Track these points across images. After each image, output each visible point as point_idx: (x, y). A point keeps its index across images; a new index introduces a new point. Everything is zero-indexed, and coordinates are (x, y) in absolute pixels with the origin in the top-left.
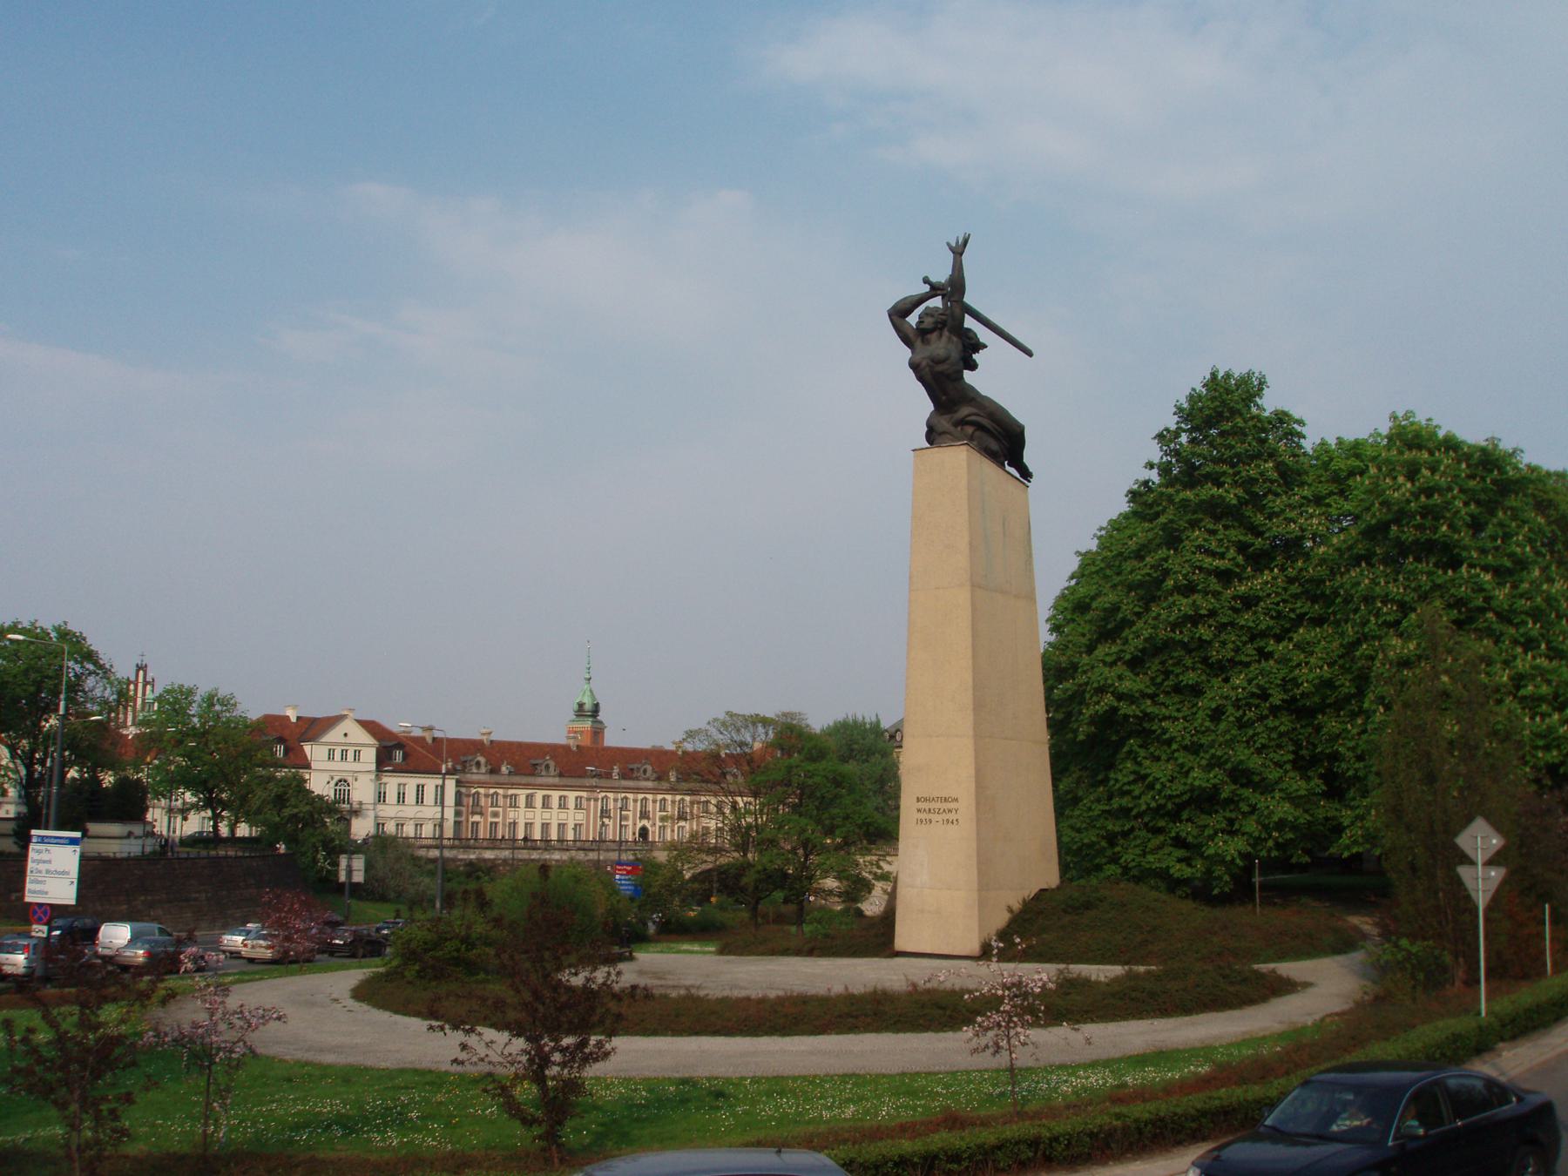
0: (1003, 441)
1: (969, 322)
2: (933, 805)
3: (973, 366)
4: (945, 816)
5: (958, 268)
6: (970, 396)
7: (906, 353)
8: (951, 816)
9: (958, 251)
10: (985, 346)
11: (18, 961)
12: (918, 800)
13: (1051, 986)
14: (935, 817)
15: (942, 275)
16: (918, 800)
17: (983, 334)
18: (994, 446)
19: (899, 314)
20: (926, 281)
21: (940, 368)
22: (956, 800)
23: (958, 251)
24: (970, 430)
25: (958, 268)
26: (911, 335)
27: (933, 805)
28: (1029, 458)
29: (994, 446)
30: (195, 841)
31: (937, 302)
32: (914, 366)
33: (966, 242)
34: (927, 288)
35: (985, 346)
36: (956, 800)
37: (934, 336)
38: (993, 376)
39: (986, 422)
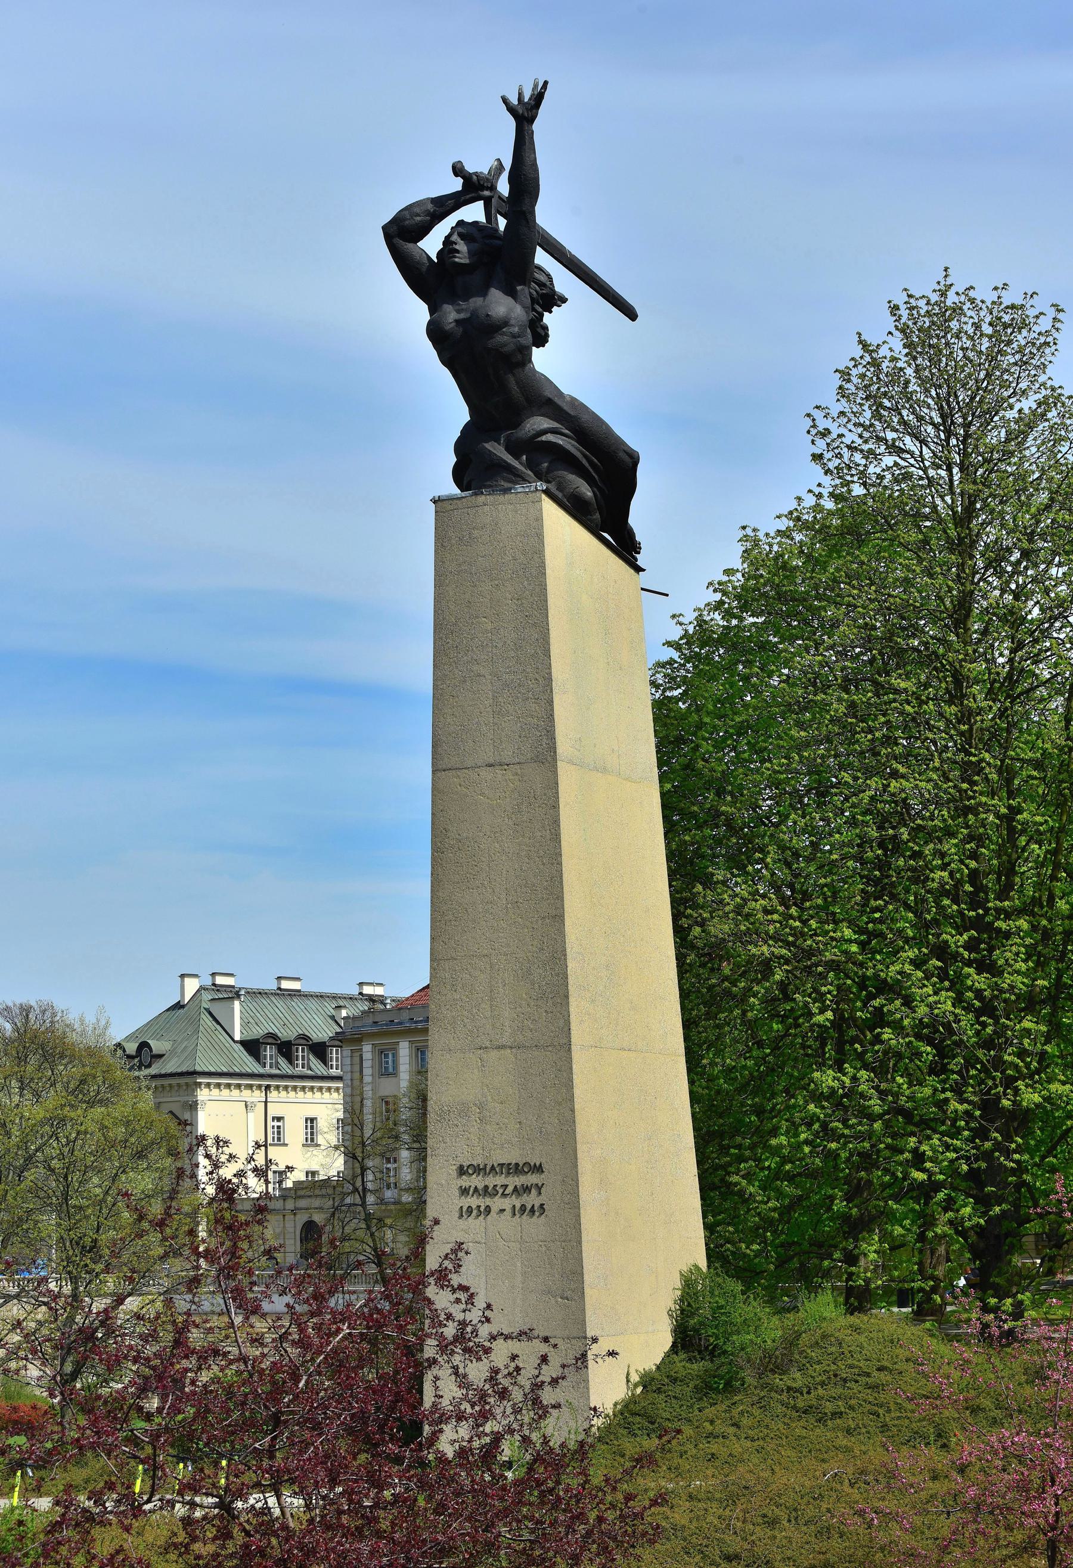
1: (542, 258)
2: (491, 1181)
6: (545, 400)
7: (419, 312)
8: (532, 1199)
9: (525, 113)
10: (564, 300)
11: (1069, 1123)
12: (462, 1171)
13: (1025, 1104)
14: (497, 1203)
15: (490, 149)
16: (462, 1171)
17: (563, 280)
18: (587, 492)
19: (402, 233)
20: (458, 170)
22: (538, 1169)
23: (525, 113)
27: (491, 1181)
28: (640, 516)
29: (587, 492)
31: (474, 212)
32: (435, 332)
33: (538, 98)
34: (456, 185)
35: (564, 300)
36: (538, 1169)
38: (574, 356)
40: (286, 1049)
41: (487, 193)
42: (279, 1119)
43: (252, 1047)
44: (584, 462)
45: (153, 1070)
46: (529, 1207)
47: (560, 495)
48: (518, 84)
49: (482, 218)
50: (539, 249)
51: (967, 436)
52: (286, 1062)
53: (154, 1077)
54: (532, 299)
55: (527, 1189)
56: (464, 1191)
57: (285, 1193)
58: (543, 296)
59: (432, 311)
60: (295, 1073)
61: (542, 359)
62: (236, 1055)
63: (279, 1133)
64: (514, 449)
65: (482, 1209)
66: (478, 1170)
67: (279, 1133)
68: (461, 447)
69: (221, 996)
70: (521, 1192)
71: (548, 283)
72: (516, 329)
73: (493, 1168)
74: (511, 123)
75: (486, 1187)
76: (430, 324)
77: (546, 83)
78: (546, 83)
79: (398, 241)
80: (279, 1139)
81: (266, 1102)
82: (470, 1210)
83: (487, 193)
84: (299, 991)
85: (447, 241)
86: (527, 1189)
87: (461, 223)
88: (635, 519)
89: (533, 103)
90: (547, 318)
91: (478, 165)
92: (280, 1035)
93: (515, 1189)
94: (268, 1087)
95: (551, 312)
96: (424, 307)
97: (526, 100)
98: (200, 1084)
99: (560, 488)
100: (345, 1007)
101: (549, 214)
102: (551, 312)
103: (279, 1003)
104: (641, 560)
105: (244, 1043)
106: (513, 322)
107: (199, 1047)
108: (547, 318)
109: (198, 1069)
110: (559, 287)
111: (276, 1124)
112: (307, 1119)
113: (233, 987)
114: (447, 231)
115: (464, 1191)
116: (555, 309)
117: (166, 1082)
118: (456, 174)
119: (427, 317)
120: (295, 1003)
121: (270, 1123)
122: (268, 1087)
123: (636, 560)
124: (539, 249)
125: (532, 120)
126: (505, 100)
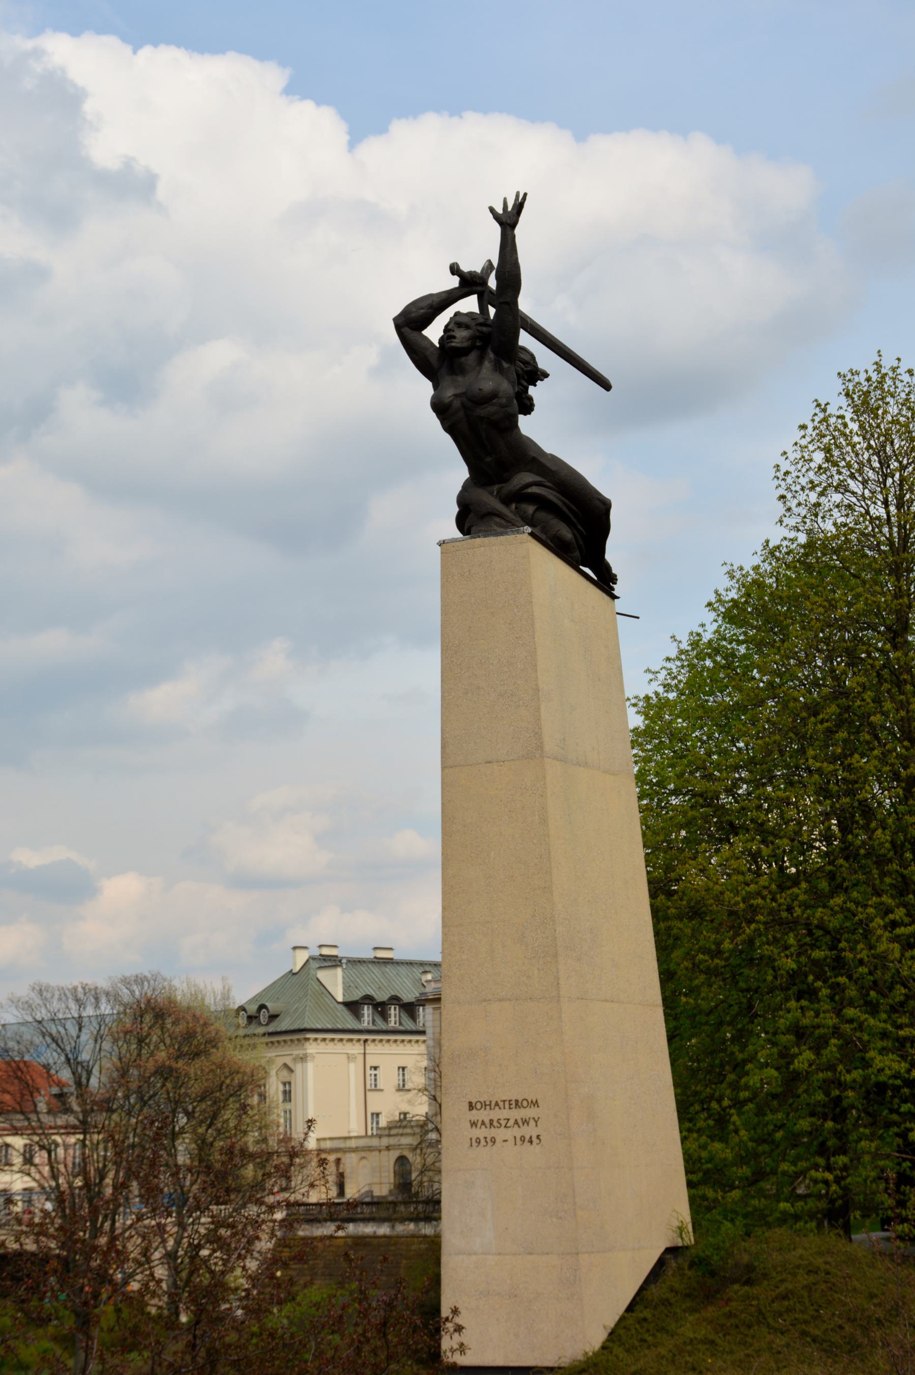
0: (576, 524)
1: (525, 340)
2: (496, 1114)
3: (527, 407)
4: (517, 1132)
5: (508, 246)
6: (529, 457)
7: (425, 388)
8: (529, 1131)
9: (508, 220)
10: (546, 375)
12: (471, 1106)
14: (501, 1134)
15: (481, 251)
17: (544, 358)
18: (567, 533)
19: (410, 323)
20: (455, 269)
21: (483, 411)
22: (535, 1104)
23: (508, 220)
24: (530, 509)
25: (508, 246)
26: (434, 360)
27: (496, 1114)
29: (567, 533)
30: (385, 1236)
31: (469, 305)
32: (439, 407)
33: (519, 207)
34: (454, 282)
35: (546, 375)
36: (535, 1104)
37: (472, 358)
38: (555, 422)
39: (551, 495)
40: (381, 1008)
41: (479, 289)
42: (375, 1068)
43: (353, 1007)
44: (565, 509)
45: (271, 1029)
46: (527, 1138)
47: (544, 537)
48: (501, 195)
49: (476, 309)
50: (522, 332)
51: (902, 479)
52: (381, 1019)
53: (271, 1034)
54: (518, 375)
55: (526, 1122)
56: (473, 1124)
57: (380, 1132)
58: (527, 372)
59: (435, 387)
60: (389, 1029)
61: (526, 425)
62: (339, 1014)
63: (375, 1080)
64: (506, 500)
65: (488, 1140)
66: (484, 1105)
67: (375, 1080)
68: (463, 501)
69: (326, 964)
70: (521, 1124)
71: (532, 362)
72: (504, 400)
73: (497, 1104)
74: (497, 229)
75: (491, 1121)
76: (433, 398)
77: (525, 195)
78: (525, 195)
79: (406, 330)
80: (376, 1085)
81: (365, 1054)
82: (478, 1141)
83: (479, 289)
84: (392, 959)
85: (447, 329)
86: (526, 1122)
87: (457, 314)
88: (611, 555)
89: (515, 212)
90: (532, 391)
91: (472, 264)
92: (375, 996)
93: (516, 1122)
94: (366, 1041)
95: (535, 385)
96: (429, 384)
97: (510, 209)
98: (308, 1039)
99: (544, 530)
100: (430, 972)
101: (525, 304)
102: (535, 385)
103: (375, 969)
104: (618, 589)
105: (347, 1004)
106: (500, 394)
107: (307, 1008)
108: (532, 391)
109: (306, 1025)
110: (541, 365)
111: (373, 1072)
112: (399, 1068)
113: (336, 956)
114: (447, 320)
115: (473, 1124)
116: (539, 383)
117: (275, 1039)
118: (453, 273)
119: (431, 392)
120: (389, 969)
121: (368, 1072)
122: (366, 1041)
123: (613, 589)
124: (522, 332)
125: (514, 226)
126: (492, 210)
